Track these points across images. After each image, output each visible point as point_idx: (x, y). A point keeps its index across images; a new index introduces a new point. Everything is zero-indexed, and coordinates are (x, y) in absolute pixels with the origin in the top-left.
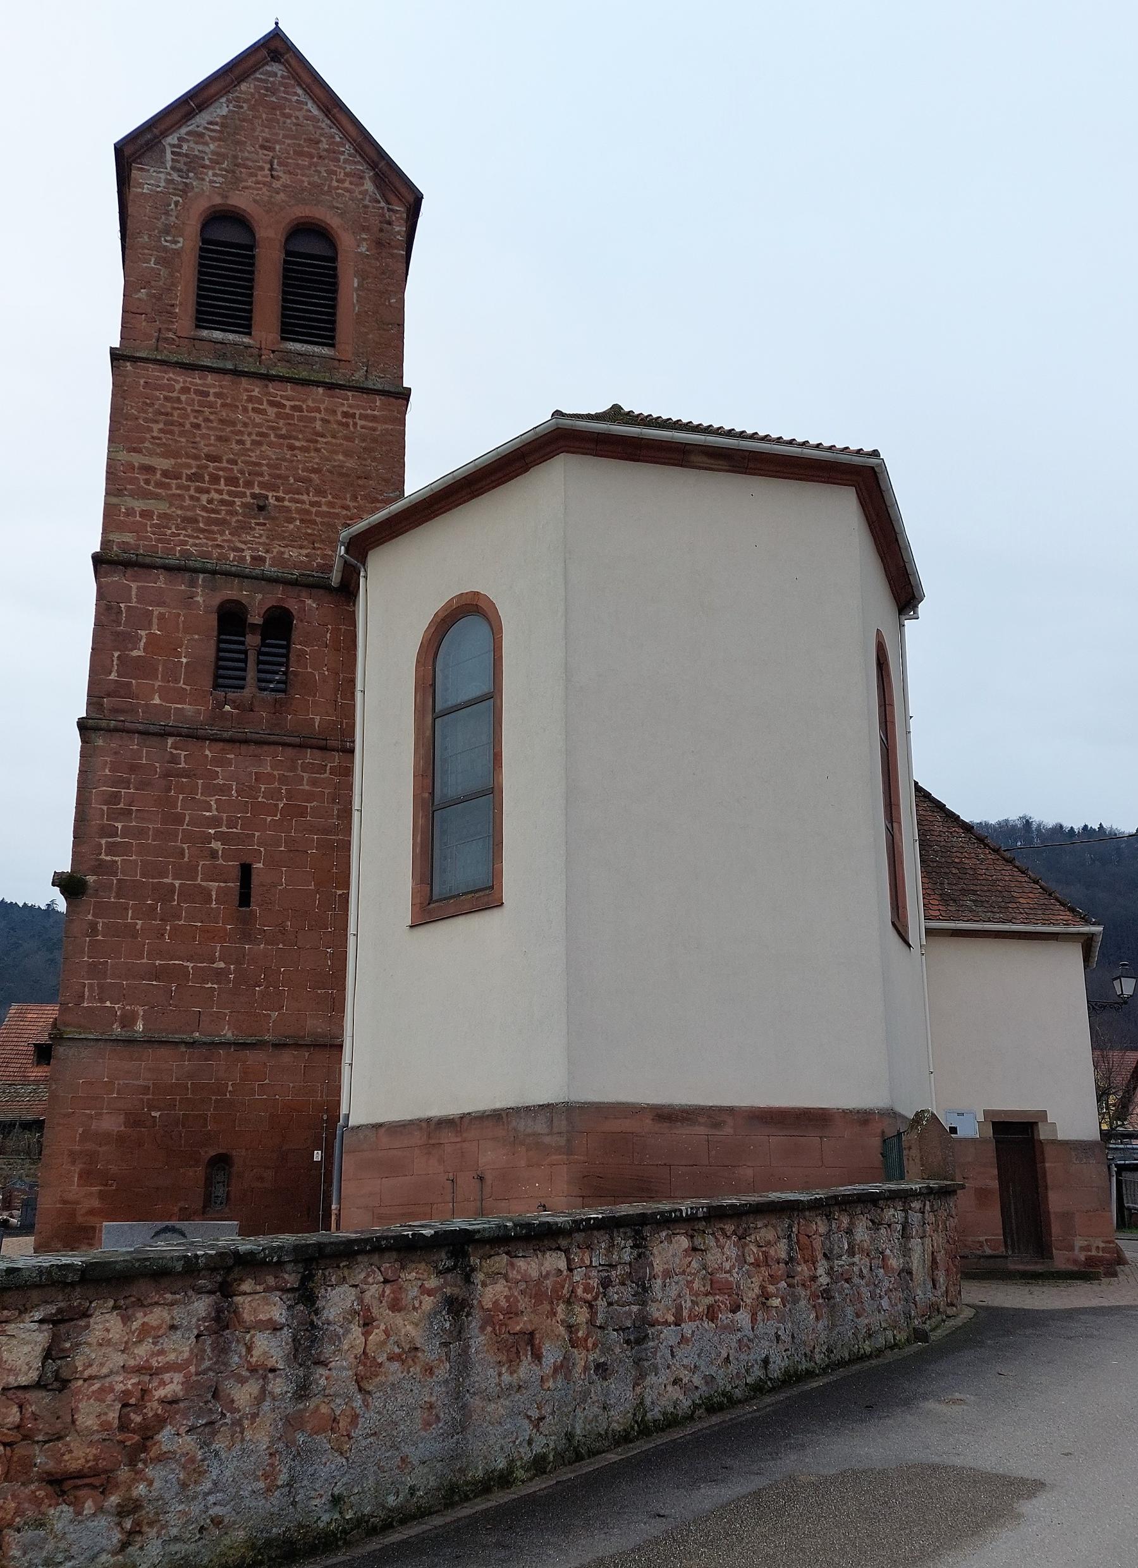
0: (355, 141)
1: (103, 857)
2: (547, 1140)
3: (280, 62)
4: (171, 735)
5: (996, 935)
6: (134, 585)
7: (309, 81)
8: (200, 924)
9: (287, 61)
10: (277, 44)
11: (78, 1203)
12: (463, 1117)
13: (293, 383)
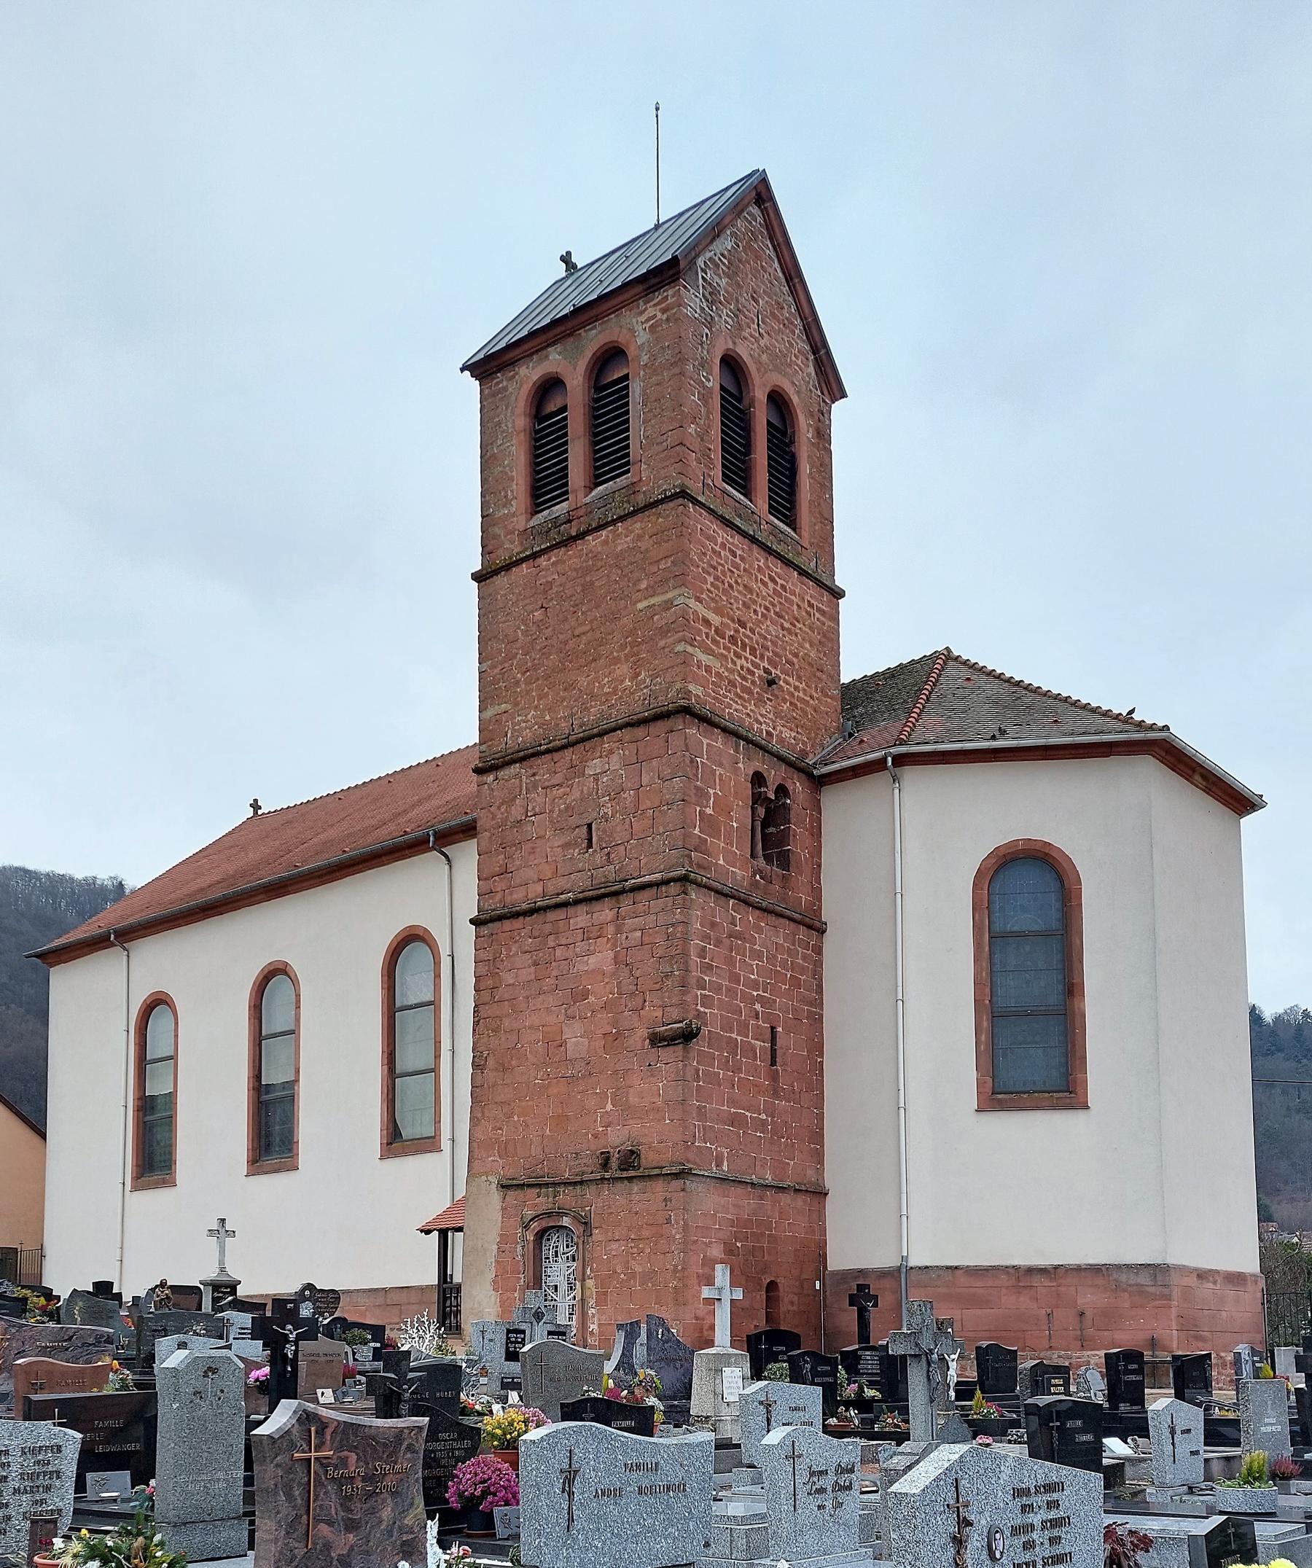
0: (806, 319)
1: (699, 1007)
2: (1152, 1289)
3: (759, 207)
4: (733, 897)
5: (142, 1046)
6: (705, 741)
7: (781, 240)
8: (752, 1078)
9: (766, 208)
10: (761, 188)
11: (703, 1319)
12: (1056, 1268)
13: (785, 563)
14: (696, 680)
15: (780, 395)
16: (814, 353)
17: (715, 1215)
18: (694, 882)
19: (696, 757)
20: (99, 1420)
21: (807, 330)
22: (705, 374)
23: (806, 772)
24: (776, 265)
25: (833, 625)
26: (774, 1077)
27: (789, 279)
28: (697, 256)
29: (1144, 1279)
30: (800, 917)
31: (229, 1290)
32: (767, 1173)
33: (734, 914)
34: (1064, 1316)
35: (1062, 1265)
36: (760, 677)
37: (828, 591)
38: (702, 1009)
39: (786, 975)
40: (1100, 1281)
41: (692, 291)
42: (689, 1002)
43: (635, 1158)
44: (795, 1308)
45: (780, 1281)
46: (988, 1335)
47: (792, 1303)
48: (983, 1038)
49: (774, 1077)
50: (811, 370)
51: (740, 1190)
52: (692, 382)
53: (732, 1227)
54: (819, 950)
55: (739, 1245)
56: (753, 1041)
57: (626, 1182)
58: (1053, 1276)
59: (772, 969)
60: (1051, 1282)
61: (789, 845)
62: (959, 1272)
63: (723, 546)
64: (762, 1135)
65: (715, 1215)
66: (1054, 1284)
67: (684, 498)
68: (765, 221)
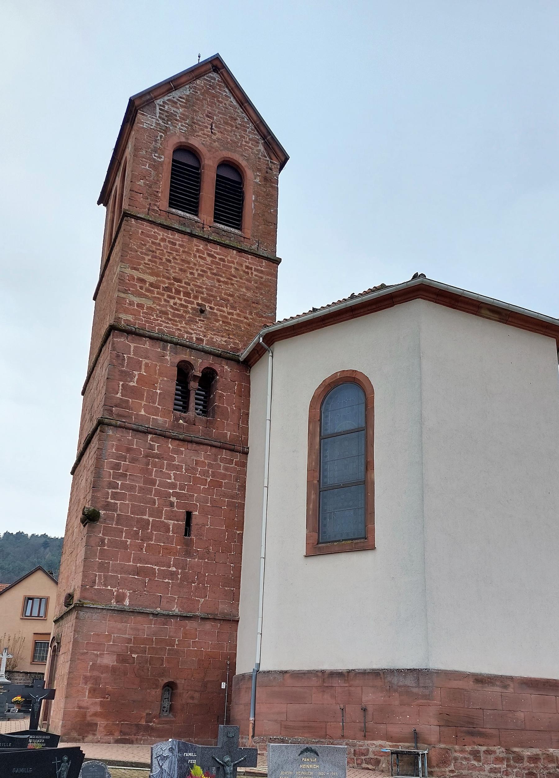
1: (109, 500)
2: (415, 690)
3: (218, 73)
4: (150, 433)
6: (132, 345)
9: (222, 73)
11: (87, 708)
12: (349, 672)
13: (221, 246)
14: (126, 311)
15: (227, 161)
16: (264, 139)
17: (110, 635)
18: (109, 425)
19: (123, 354)
20: (305, 758)
21: (257, 128)
22: (157, 155)
23: (232, 359)
24: (232, 99)
25: (270, 278)
26: (188, 544)
27: (241, 104)
28: (156, 98)
29: (410, 681)
30: (219, 444)
31: (3, 687)
32: (174, 607)
33: (152, 443)
34: (353, 711)
35: (354, 670)
36: (193, 309)
37: (265, 259)
38: (112, 501)
39: (206, 480)
40: (379, 683)
41: (149, 116)
42: (98, 496)
43: (71, 599)
44: (196, 702)
45: (180, 683)
46: (303, 725)
47: (192, 698)
48: (311, 506)
49: (188, 544)
50: (261, 147)
51: (140, 618)
52: (144, 159)
53: (128, 643)
54: (244, 465)
55: (135, 656)
56: (166, 521)
57: (151, 617)
58: (346, 679)
59: (190, 476)
60: (345, 683)
61: (215, 403)
62: (287, 675)
63: (163, 240)
64: (170, 581)
65: (110, 635)
66: (347, 685)
67: (127, 217)
68: (222, 79)
